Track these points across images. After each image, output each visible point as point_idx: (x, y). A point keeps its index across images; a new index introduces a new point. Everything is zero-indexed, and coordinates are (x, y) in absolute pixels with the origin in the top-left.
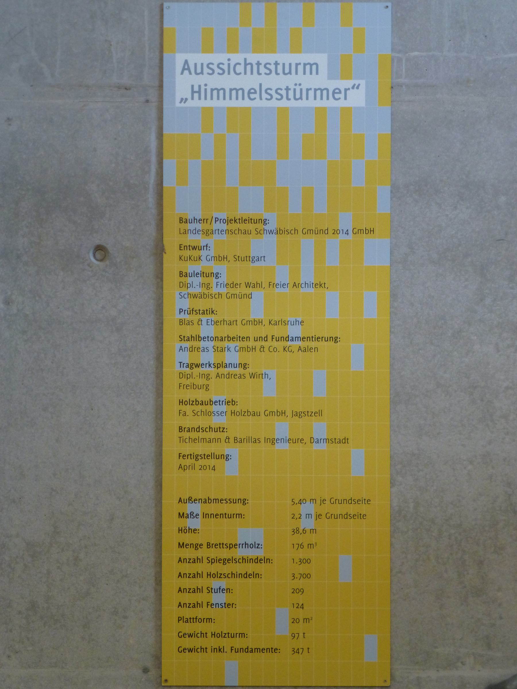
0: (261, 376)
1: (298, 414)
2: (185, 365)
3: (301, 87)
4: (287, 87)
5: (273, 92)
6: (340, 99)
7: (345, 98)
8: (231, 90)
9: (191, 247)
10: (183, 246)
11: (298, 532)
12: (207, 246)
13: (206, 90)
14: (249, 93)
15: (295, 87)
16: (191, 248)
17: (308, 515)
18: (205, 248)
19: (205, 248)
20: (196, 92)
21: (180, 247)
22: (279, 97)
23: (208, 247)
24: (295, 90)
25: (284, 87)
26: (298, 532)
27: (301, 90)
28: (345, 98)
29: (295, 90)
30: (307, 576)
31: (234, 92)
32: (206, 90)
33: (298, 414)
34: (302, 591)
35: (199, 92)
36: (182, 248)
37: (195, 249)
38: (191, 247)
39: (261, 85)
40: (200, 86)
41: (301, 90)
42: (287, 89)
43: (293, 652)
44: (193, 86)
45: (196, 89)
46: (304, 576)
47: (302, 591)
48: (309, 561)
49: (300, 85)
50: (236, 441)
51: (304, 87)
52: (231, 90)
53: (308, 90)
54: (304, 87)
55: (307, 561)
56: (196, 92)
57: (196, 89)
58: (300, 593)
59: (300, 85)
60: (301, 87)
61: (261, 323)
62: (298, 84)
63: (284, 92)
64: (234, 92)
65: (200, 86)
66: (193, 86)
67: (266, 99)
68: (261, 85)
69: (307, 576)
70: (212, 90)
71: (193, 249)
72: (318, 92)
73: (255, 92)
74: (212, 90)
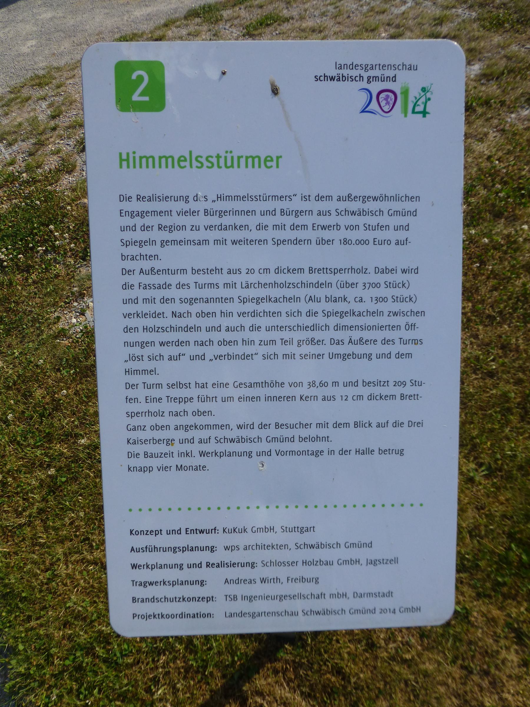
0: (272, 581)
1: (315, 453)
2: (138, 584)
3: (232, 155)
4: (218, 154)
5: (203, 160)
6: (272, 166)
7: (278, 166)
8: (160, 158)
9: (198, 531)
10: (189, 530)
11: (314, 385)
12: (215, 529)
13: (134, 158)
14: (179, 160)
15: (226, 155)
16: (198, 532)
17: (334, 383)
18: (213, 531)
19: (213, 531)
20: (125, 160)
21: (186, 531)
22: (210, 165)
23: (216, 531)
24: (226, 157)
25: (214, 155)
26: (314, 385)
27: (232, 158)
28: (278, 166)
29: (226, 157)
30: (376, 285)
31: (163, 160)
32: (134, 158)
33: (315, 453)
34: (404, 383)
35: (127, 160)
36: (189, 532)
37: (203, 533)
38: (198, 531)
39: (191, 152)
40: (128, 154)
41: (232, 158)
42: (218, 157)
43: (309, 386)
44: (121, 154)
45: (124, 157)
46: (374, 285)
47: (404, 383)
48: (378, 285)
49: (231, 152)
50: (146, 456)
51: (235, 155)
52: (160, 158)
53: (239, 158)
54: (235, 155)
55: (383, 300)
56: (125, 160)
57: (124, 157)
58: (402, 386)
59: (231, 152)
60: (232, 155)
61: (272, 530)
62: (229, 151)
63: (214, 160)
64: (163, 160)
65: (128, 154)
66: (121, 154)
67: (197, 167)
68: (191, 152)
69: (376, 285)
70: (141, 158)
71: (200, 533)
72: (250, 160)
73: (185, 160)
74: (141, 158)
